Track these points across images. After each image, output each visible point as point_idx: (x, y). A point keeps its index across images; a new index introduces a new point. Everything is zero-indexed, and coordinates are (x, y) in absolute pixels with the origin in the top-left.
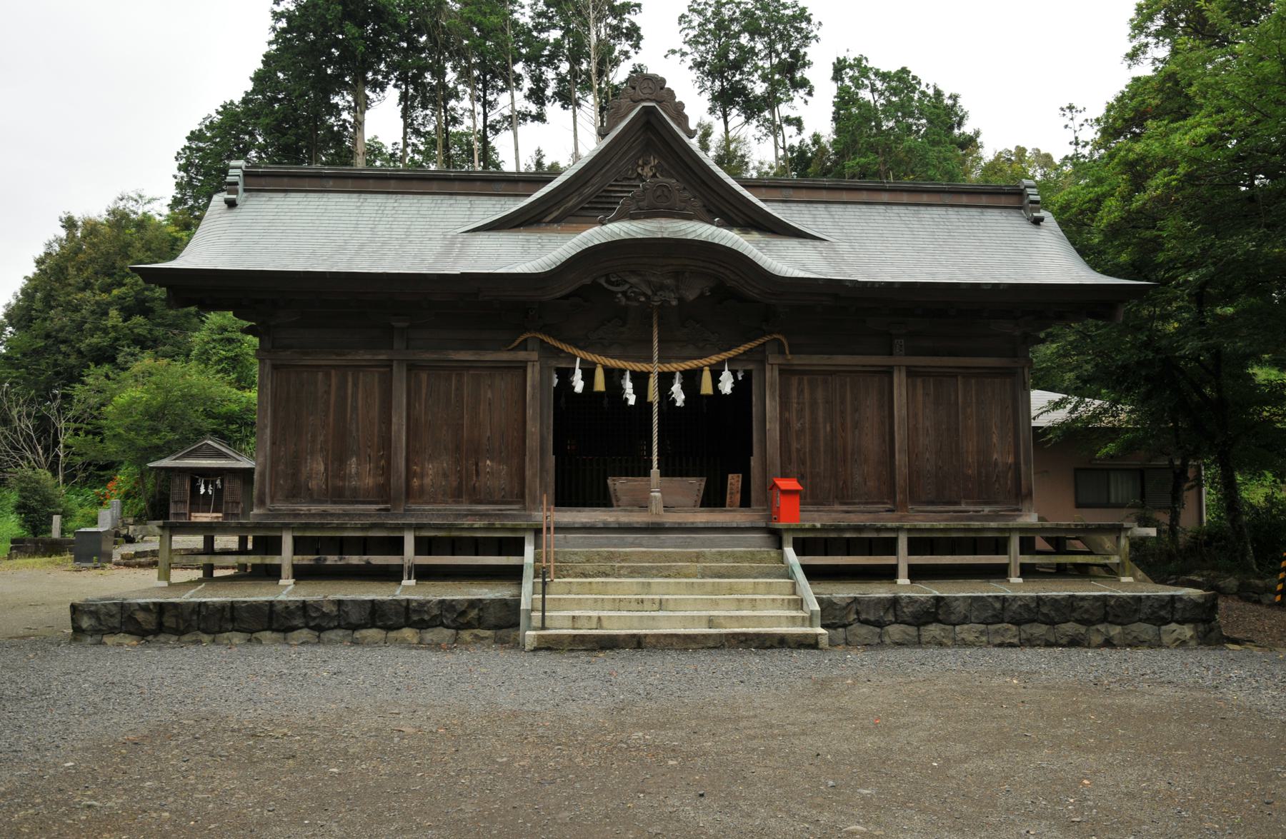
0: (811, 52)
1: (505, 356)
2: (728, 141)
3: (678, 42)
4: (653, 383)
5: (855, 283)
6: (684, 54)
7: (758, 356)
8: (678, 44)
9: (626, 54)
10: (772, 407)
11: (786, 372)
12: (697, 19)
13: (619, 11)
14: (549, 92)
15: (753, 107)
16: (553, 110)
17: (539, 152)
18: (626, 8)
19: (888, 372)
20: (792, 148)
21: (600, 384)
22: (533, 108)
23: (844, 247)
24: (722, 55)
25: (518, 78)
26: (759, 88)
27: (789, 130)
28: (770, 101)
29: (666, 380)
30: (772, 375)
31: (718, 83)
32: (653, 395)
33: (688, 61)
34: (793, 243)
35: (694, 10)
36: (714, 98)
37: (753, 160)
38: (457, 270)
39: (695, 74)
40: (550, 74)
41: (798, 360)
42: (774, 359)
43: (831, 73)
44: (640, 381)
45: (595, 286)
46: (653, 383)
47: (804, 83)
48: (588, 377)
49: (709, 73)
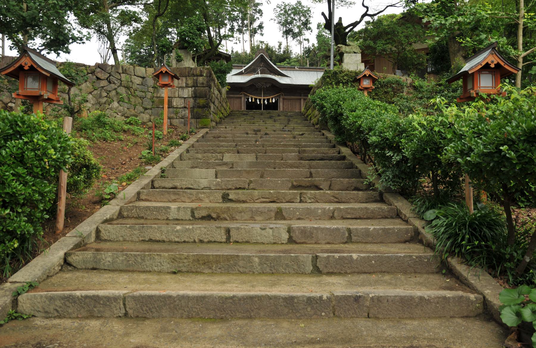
0: (311, 20)
1: (238, 96)
2: (288, 46)
3: (273, 16)
4: (262, 100)
5: (293, 85)
6: (275, 20)
7: (279, 96)
8: (274, 17)
9: (258, 18)
10: (281, 104)
11: (283, 99)
12: (279, 10)
13: (257, 5)
14: (235, 30)
15: (295, 35)
16: (236, 35)
17: (232, 48)
18: (258, 4)
19: (300, 99)
20: (306, 48)
21: (253, 101)
22: (230, 33)
23: (294, 79)
24: (286, 21)
25: (226, 25)
26: (296, 30)
27: (305, 42)
28: (300, 34)
29: (264, 100)
30: (281, 99)
31: (285, 28)
32: (262, 102)
33: (277, 22)
34: (286, 78)
35: (278, 7)
36: (284, 33)
37: (294, 52)
38: (232, 82)
39: (278, 25)
40: (235, 24)
41: (286, 97)
42: (281, 97)
43: (316, 27)
44: (260, 100)
45: (253, 85)
46: (262, 100)
47: (310, 29)
48: (252, 99)
49: (282, 25)
